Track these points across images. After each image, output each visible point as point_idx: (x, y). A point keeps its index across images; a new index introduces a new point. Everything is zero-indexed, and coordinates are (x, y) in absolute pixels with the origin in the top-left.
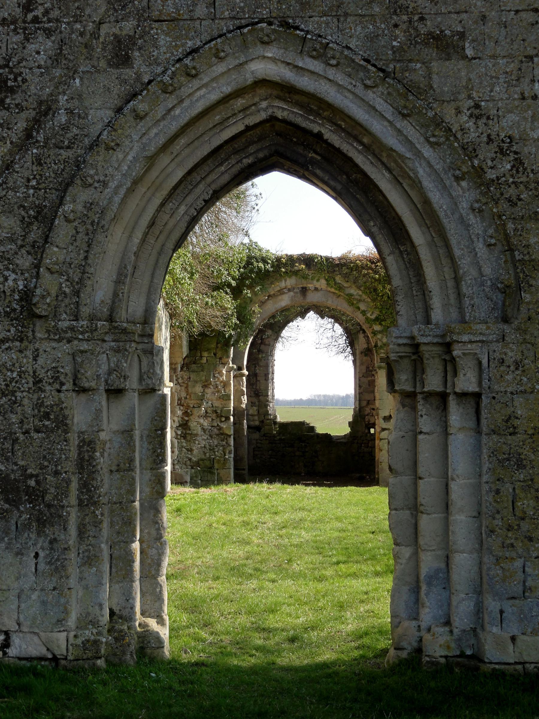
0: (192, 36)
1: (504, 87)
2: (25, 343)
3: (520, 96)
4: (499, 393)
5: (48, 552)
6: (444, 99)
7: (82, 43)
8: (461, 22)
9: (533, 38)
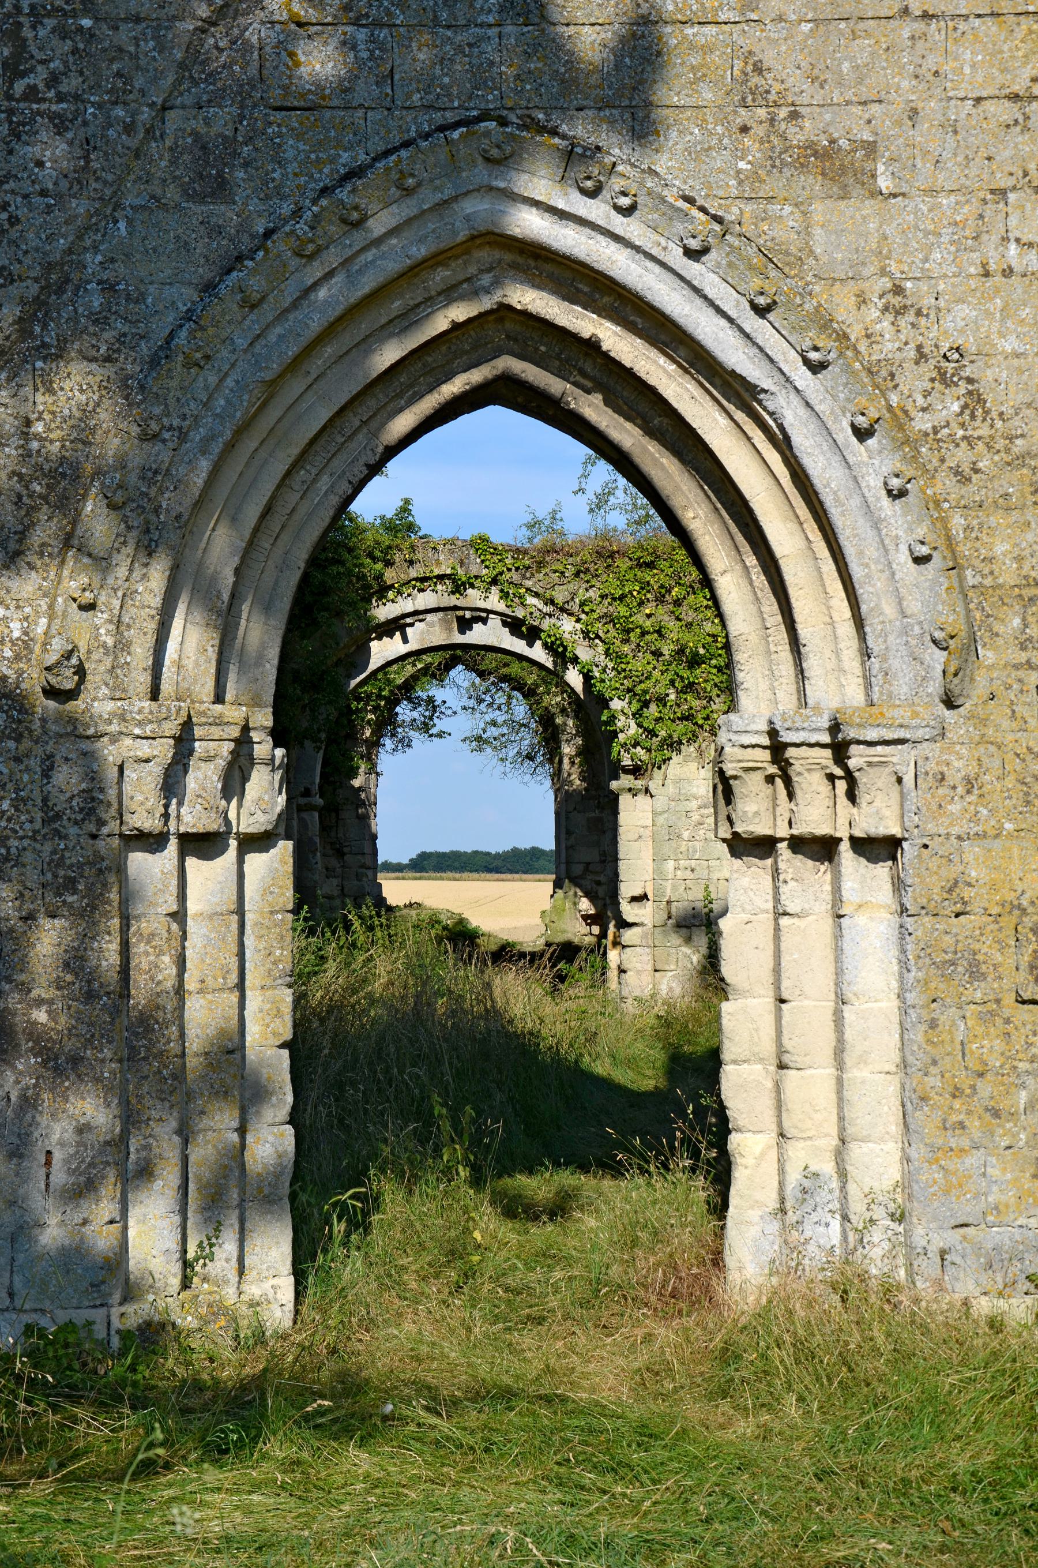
0: (349, 142)
1: (949, 253)
2: (26, 743)
3: (981, 270)
4: (936, 838)
5: (72, 1151)
6: (836, 276)
7: (128, 148)
8: (869, 122)
9: (1007, 153)
